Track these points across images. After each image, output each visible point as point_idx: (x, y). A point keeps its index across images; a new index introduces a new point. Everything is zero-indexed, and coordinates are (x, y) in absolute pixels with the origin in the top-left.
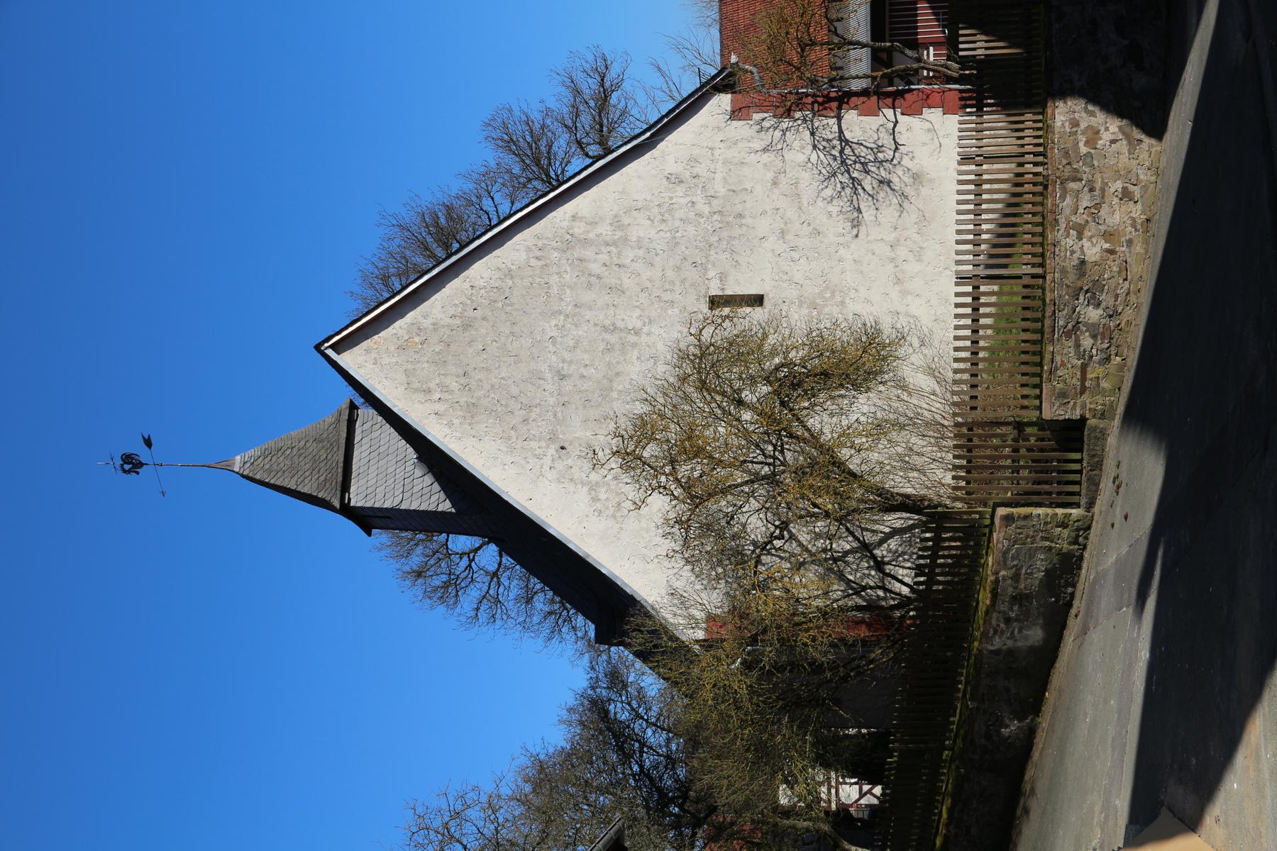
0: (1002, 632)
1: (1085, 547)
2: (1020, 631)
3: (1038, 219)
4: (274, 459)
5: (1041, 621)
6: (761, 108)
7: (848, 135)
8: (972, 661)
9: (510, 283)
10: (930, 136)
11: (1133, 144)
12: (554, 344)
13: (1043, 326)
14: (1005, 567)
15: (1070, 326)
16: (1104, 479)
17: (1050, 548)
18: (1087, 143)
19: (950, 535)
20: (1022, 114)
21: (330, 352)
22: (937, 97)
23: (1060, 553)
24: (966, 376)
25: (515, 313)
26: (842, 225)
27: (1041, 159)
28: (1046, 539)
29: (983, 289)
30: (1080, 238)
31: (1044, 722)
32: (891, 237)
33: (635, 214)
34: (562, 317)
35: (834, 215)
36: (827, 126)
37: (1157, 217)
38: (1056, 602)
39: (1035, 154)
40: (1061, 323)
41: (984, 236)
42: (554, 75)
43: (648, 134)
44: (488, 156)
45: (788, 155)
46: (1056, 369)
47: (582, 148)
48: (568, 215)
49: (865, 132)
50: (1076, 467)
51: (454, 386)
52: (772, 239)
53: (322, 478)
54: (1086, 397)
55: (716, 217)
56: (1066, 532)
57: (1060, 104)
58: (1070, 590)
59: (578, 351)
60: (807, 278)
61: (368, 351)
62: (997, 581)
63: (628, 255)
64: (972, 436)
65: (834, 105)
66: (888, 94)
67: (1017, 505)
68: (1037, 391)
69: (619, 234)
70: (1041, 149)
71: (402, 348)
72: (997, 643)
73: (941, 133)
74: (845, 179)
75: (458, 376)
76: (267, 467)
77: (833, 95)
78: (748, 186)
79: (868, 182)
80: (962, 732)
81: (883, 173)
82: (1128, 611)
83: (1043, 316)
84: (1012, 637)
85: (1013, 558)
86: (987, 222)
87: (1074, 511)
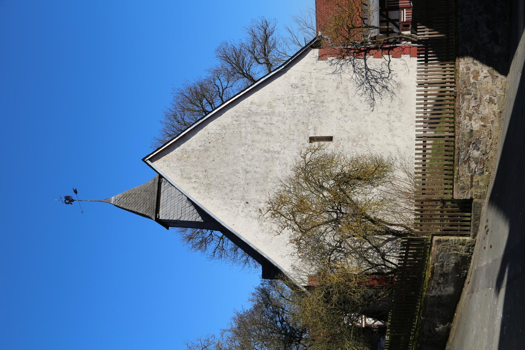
0: (436, 288)
2: (444, 288)
3: (452, 111)
4: (128, 198)
5: (453, 284)
6: (331, 55)
7: (369, 66)
8: (423, 300)
10: (404, 67)
11: (494, 78)
13: (454, 158)
14: (437, 262)
15: (466, 159)
16: (480, 225)
17: (457, 254)
18: (474, 78)
19: (414, 246)
20: (445, 64)
21: (149, 162)
22: (407, 50)
25: (227, 145)
26: (366, 106)
27: (453, 85)
28: (455, 250)
29: (428, 142)
30: (470, 120)
32: (388, 111)
33: (277, 101)
34: (247, 146)
35: (363, 101)
37: (504, 111)
38: (460, 276)
39: (451, 83)
40: (462, 157)
41: (428, 110)
42: (245, 29)
43: (283, 67)
44: (217, 63)
45: (343, 76)
47: (257, 60)
48: (249, 102)
49: (376, 65)
50: (468, 219)
51: (201, 176)
52: (336, 112)
53: (148, 207)
54: (473, 190)
55: (312, 103)
56: (464, 247)
57: (462, 60)
58: (466, 271)
59: (254, 161)
61: (165, 161)
62: (433, 268)
63: (275, 119)
64: (423, 204)
65: (363, 53)
66: (386, 49)
67: (442, 235)
69: (271, 110)
70: (453, 80)
71: (179, 160)
72: (434, 293)
73: (409, 66)
74: (368, 86)
75: (203, 172)
76: (125, 202)
77: (362, 49)
78: (326, 89)
79: (377, 87)
80: (418, 329)
81: (384, 83)
82: (492, 290)
84: (440, 290)
85: (441, 258)
87: (467, 238)
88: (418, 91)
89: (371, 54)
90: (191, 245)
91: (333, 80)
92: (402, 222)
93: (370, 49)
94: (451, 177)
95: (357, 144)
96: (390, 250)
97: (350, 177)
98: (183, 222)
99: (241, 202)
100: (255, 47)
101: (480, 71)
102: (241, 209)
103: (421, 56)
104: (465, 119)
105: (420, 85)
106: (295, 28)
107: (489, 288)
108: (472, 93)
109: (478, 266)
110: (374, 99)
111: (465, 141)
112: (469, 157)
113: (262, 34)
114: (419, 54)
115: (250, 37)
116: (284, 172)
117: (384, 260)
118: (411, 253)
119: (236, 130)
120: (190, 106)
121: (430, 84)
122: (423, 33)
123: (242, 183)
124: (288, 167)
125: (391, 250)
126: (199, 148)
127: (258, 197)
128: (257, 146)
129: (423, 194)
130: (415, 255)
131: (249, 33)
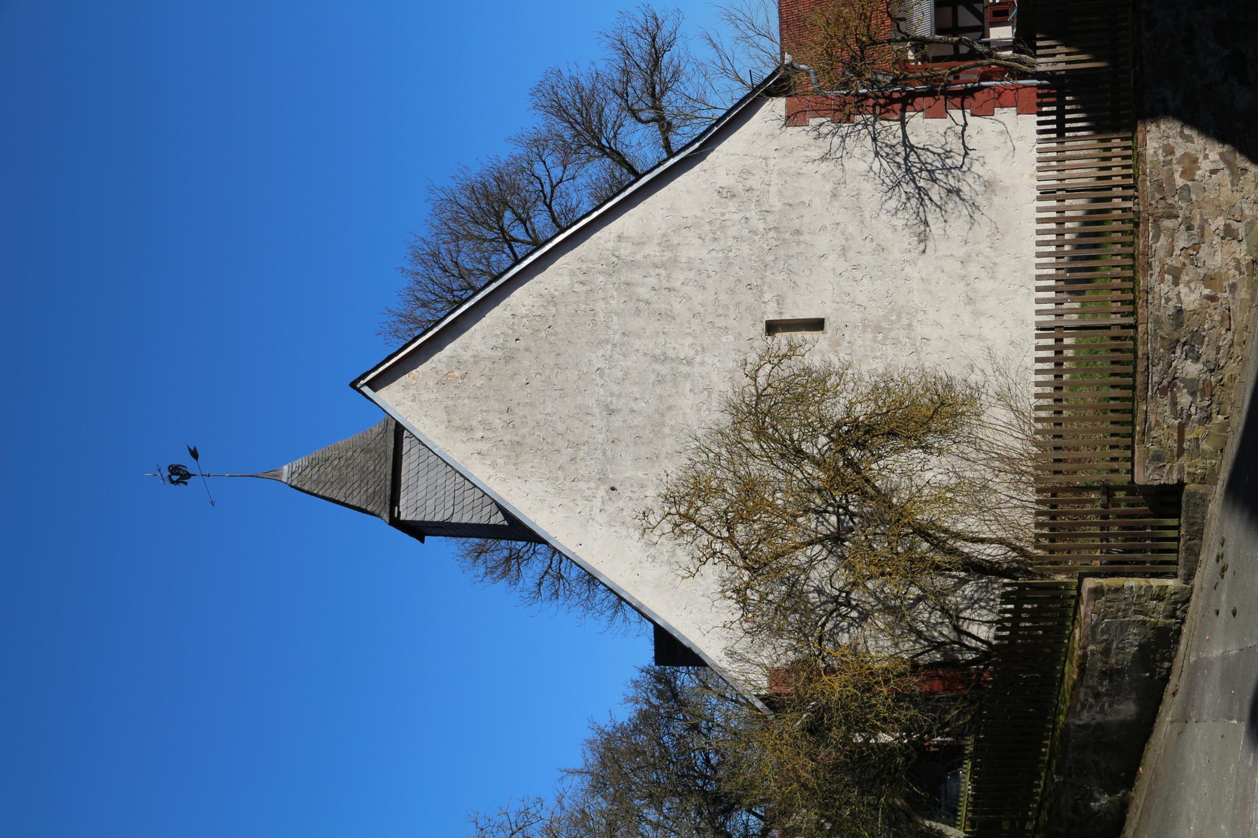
0: (1091, 707)
1: (1183, 621)
2: (1110, 706)
4: (322, 469)
5: (1134, 696)
6: (817, 112)
7: (913, 140)
9: (553, 310)
10: (1002, 139)
11: (1237, 173)
12: (602, 376)
13: (1135, 381)
14: (1094, 641)
15: (1165, 382)
17: (1144, 622)
18: (1183, 174)
19: (1037, 604)
20: (1109, 140)
21: (366, 390)
23: (1154, 627)
24: (1049, 390)
26: (908, 240)
27: (1131, 192)
28: (1140, 613)
29: (1067, 341)
30: (1176, 283)
31: (1139, 798)
32: (961, 252)
35: (899, 228)
36: (890, 129)
38: (1151, 677)
39: (1125, 187)
40: (1156, 379)
41: (1067, 236)
43: (697, 145)
44: (536, 122)
45: (848, 164)
46: (1150, 429)
48: (613, 236)
50: (1173, 533)
51: (497, 423)
52: (832, 257)
53: (371, 491)
54: (1184, 461)
55: (771, 234)
56: (1162, 605)
57: (1152, 127)
58: (1166, 665)
60: (871, 299)
61: (406, 387)
62: (1085, 656)
63: (679, 277)
64: (1057, 505)
65: (898, 106)
66: (956, 94)
68: (1129, 453)
69: (668, 254)
72: (1085, 717)
73: (1014, 136)
74: (910, 188)
75: (501, 413)
76: (315, 477)
77: (896, 95)
78: (806, 199)
79: (935, 192)
80: (1047, 804)
81: (952, 181)
83: (1135, 371)
84: (1102, 711)
85: (1103, 632)
86: (1071, 219)
87: (1171, 583)
88: (1039, 210)
89: (918, 107)
90: (483, 570)
91: (824, 175)
92: (1001, 534)
93: (914, 95)
94: (1129, 429)
95: (885, 338)
96: (972, 603)
97: (870, 430)
98: (459, 525)
99: (597, 488)
100: (628, 81)
101: (1201, 157)
102: (597, 503)
103: (1044, 109)
104: (1162, 281)
105: (1045, 193)
106: (726, 35)
107: (1230, 718)
108: (1181, 213)
109: (1198, 656)
110: (926, 223)
111: (1162, 338)
112: (1175, 378)
113: (646, 47)
114: (1040, 105)
115: (616, 56)
116: (704, 414)
117: (957, 629)
118: (1027, 610)
119: (583, 307)
120: (474, 230)
121: (1073, 192)
122: (1051, 59)
123: (600, 440)
124: (715, 396)
125: (976, 602)
126: (490, 353)
127: (640, 474)
128: (636, 347)
129: (1056, 472)
130: (1034, 616)
131: (613, 46)
